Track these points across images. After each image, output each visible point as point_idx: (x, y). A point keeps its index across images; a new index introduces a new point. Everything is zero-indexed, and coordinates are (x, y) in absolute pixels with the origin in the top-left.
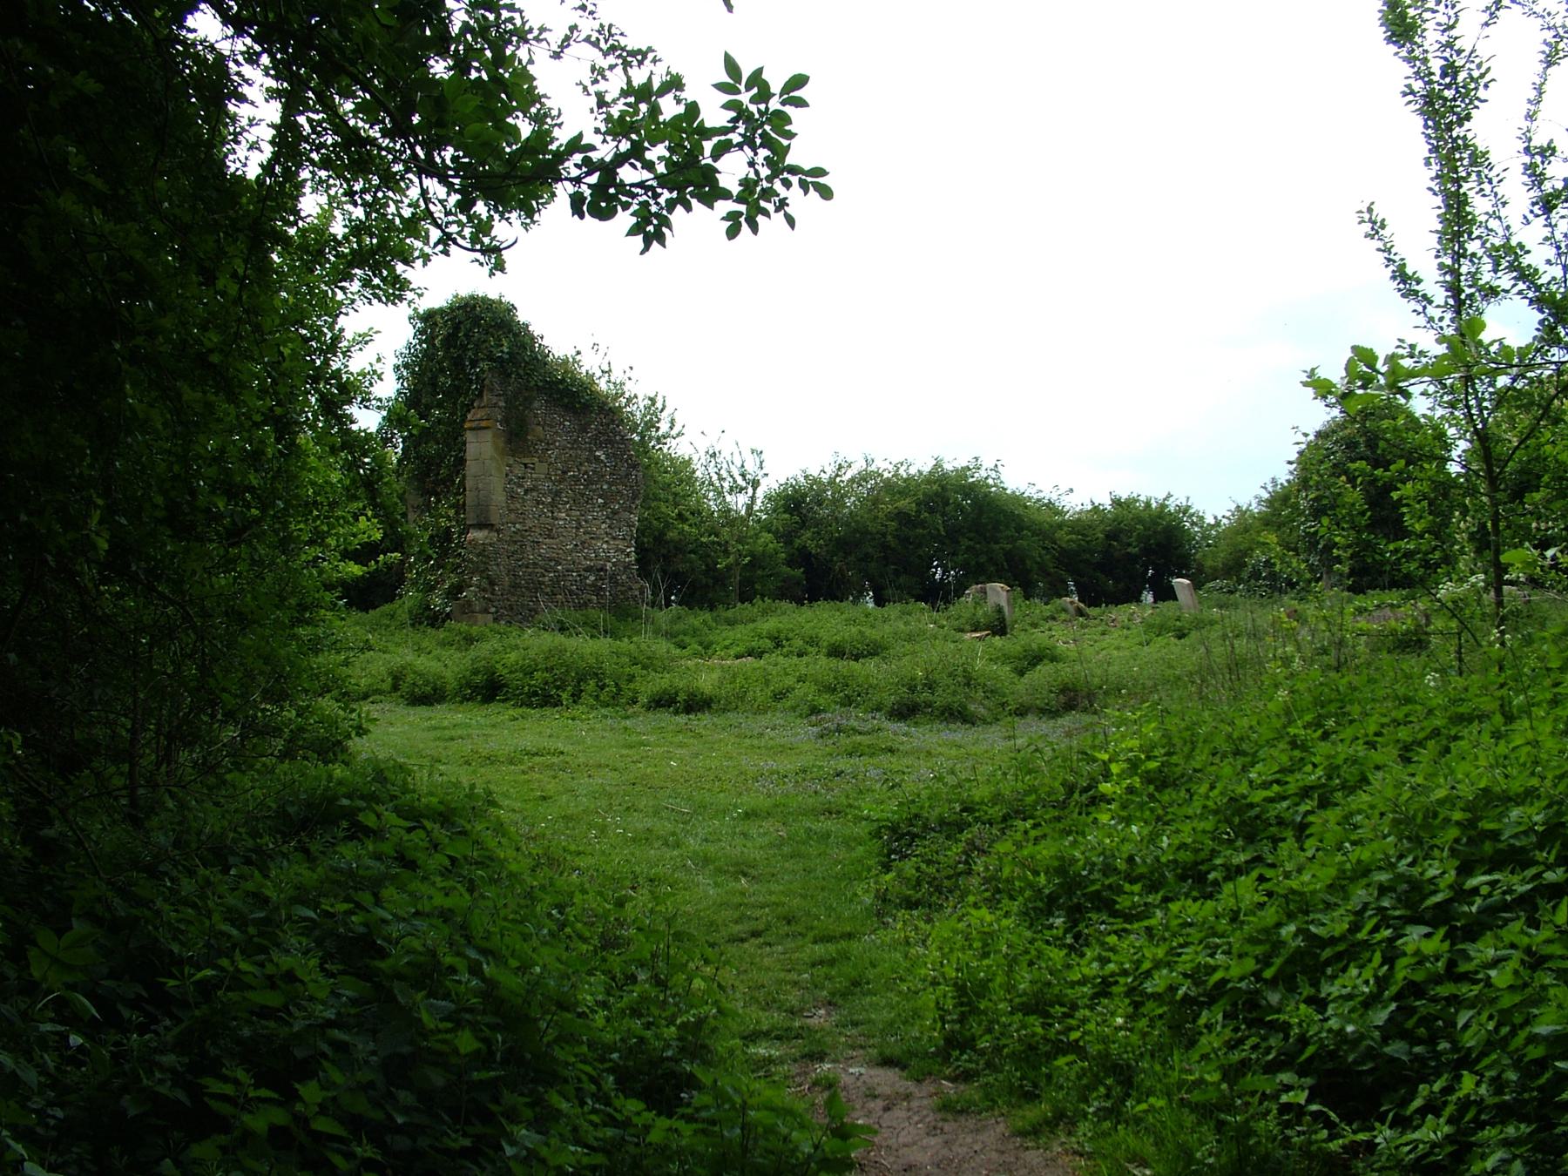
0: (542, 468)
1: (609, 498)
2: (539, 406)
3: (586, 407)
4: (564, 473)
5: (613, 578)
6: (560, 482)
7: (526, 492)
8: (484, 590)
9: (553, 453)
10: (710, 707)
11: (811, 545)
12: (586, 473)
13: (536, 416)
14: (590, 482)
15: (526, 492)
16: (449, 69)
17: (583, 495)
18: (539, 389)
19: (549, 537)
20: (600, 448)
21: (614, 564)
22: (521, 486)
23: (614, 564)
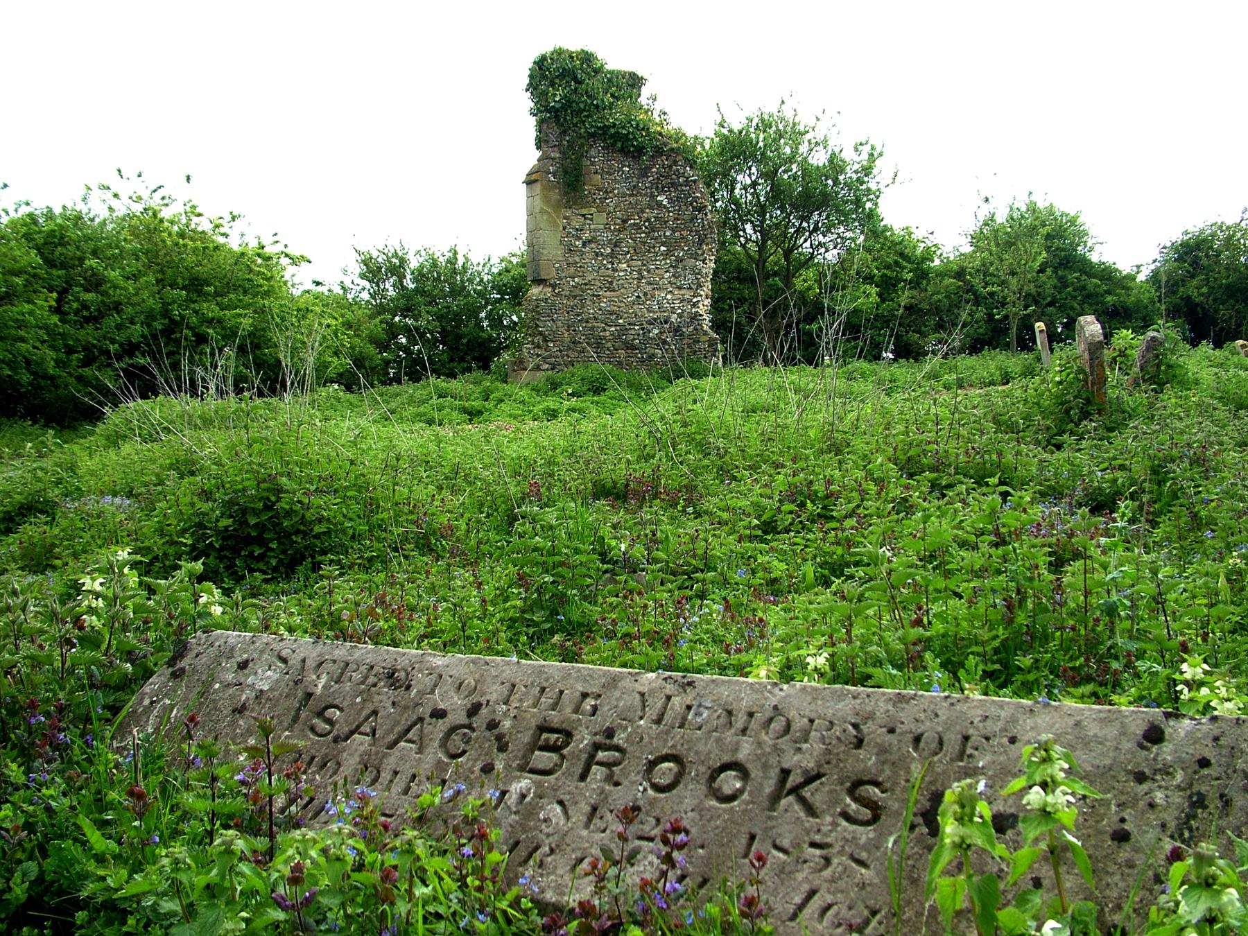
0: (601, 218)
1: (672, 245)
2: (597, 155)
3: (640, 150)
4: (625, 221)
5: (677, 330)
6: (620, 231)
7: (584, 245)
8: (538, 347)
9: (611, 202)
10: (485, 366)
11: (1194, 293)
12: (648, 220)
13: (593, 164)
14: (653, 229)
15: (584, 245)
16: (83, 584)
17: (644, 243)
18: (593, 135)
19: (609, 289)
20: (662, 192)
21: (680, 316)
22: (580, 238)
23: (680, 316)
